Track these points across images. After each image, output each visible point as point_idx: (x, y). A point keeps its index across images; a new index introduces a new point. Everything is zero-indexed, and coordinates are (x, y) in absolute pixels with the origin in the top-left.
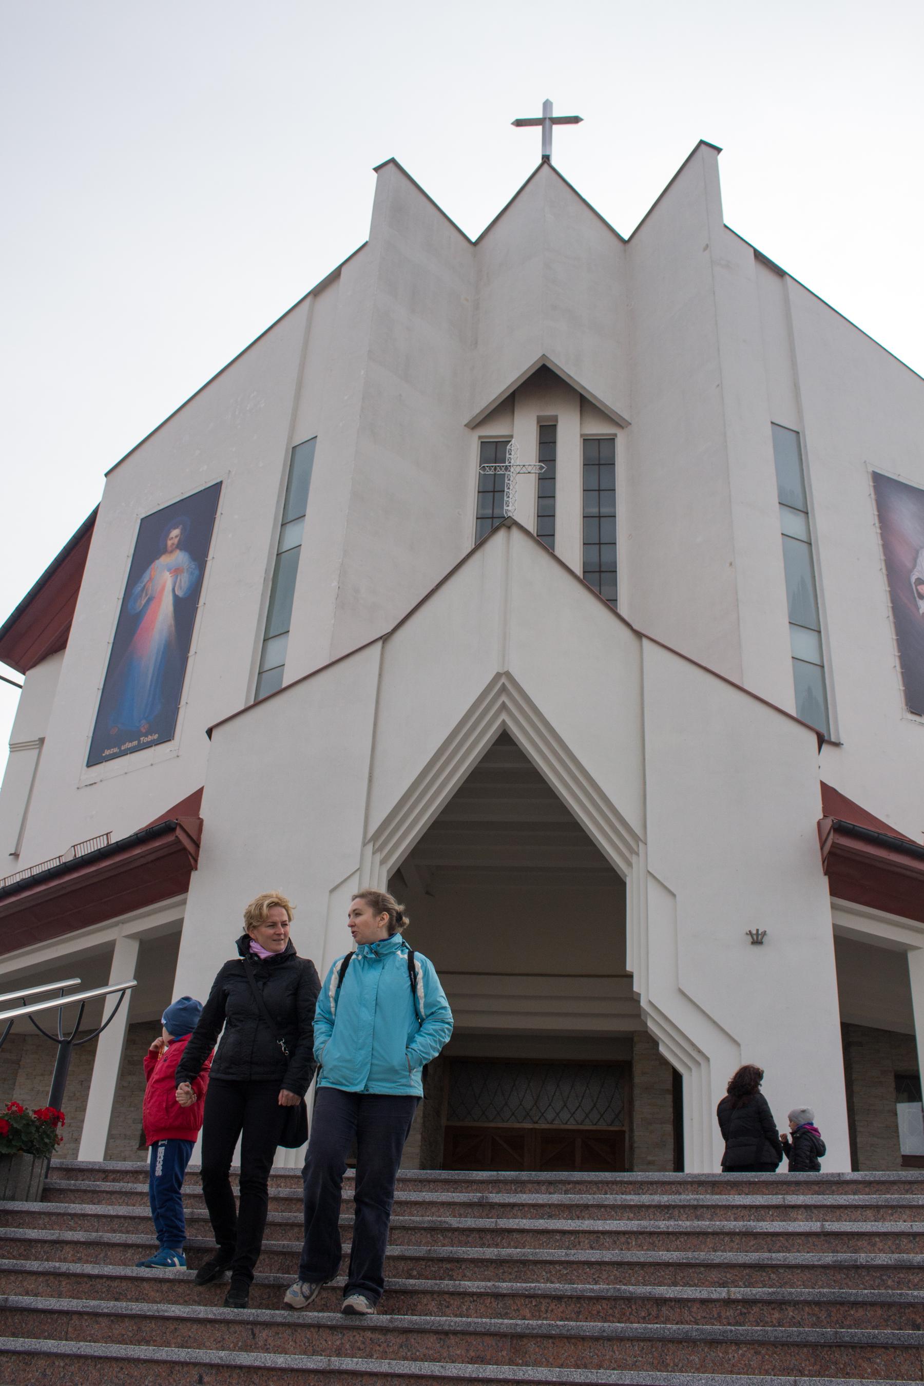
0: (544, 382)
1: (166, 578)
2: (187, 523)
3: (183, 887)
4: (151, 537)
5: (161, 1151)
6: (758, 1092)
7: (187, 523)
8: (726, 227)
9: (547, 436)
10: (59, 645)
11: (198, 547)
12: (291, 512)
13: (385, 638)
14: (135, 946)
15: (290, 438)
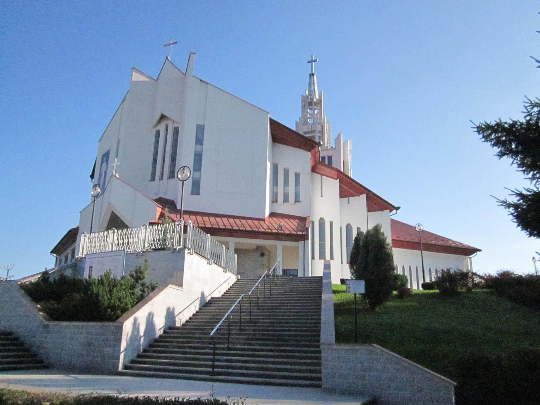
0: (163, 117)
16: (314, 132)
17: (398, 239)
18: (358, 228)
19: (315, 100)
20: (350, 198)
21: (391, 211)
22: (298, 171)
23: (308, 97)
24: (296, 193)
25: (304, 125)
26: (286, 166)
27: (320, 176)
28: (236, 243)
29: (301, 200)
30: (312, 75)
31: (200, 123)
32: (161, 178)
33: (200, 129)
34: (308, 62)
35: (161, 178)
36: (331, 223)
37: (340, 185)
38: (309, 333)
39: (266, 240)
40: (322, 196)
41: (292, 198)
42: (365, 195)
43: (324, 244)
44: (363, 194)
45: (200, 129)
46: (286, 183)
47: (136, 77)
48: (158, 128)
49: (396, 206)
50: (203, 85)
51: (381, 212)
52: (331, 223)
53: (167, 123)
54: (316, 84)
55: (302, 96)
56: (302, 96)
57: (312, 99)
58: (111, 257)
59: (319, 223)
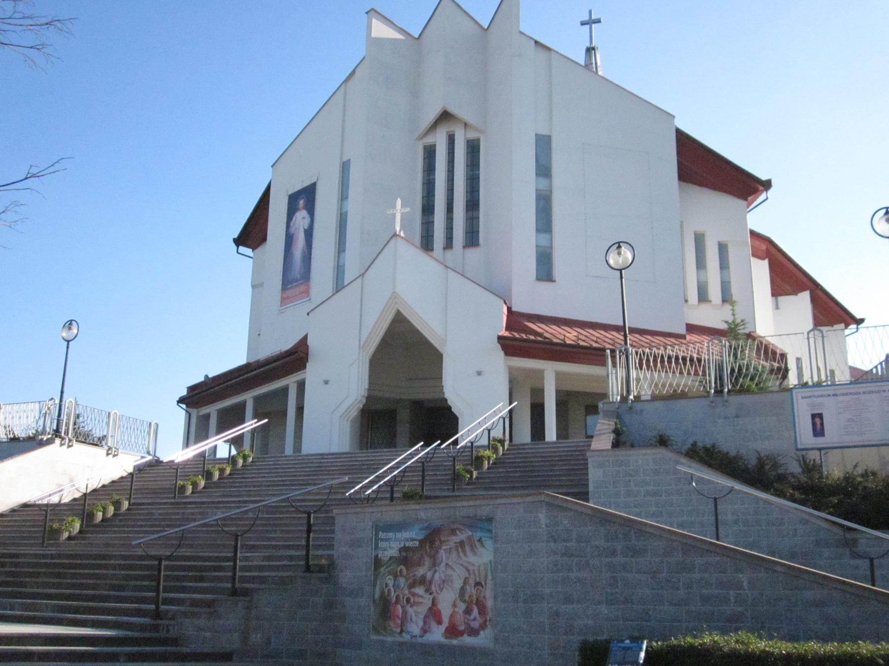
0: (445, 116)
1: (301, 217)
2: (305, 198)
3: (305, 367)
4: (293, 200)
5: (289, 450)
6: (178, 464)
7: (305, 198)
8: (521, 32)
9: (451, 140)
10: (264, 239)
11: (310, 209)
12: (344, 196)
13: (363, 275)
14: (296, 385)
15: (341, 158)
21: (847, 326)
22: (723, 239)
24: (722, 282)
26: (699, 228)
28: (559, 375)
31: (544, 132)
32: (449, 243)
33: (544, 144)
34: (583, 24)
35: (449, 243)
38: (278, 516)
41: (715, 293)
44: (805, 290)
45: (544, 144)
49: (858, 316)
50: (542, 54)
53: (452, 129)
58: (840, 398)
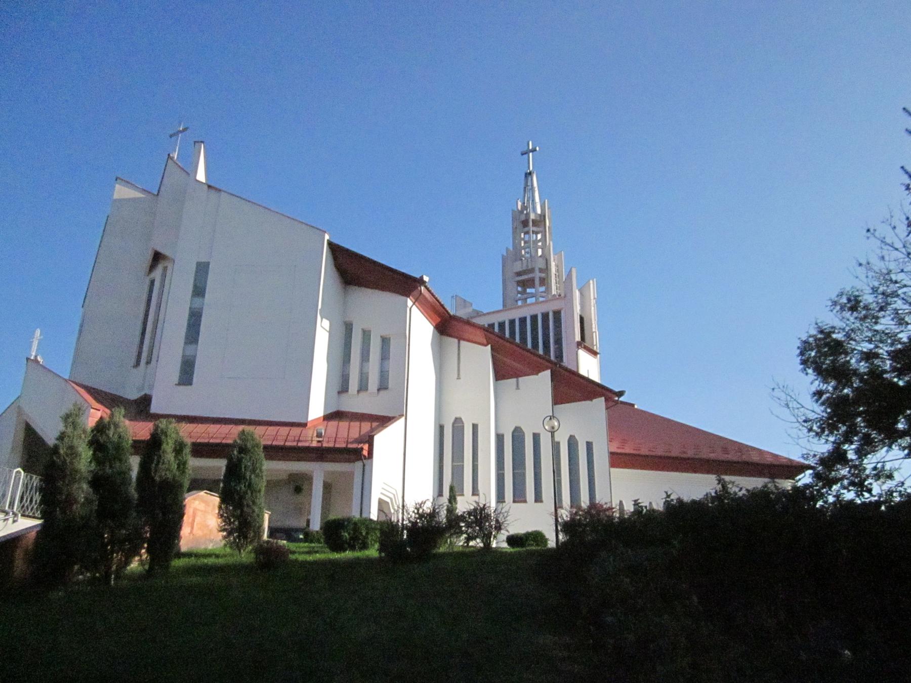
16: (532, 270)
17: (634, 452)
18: (587, 443)
19: (532, 216)
20: (520, 379)
22: (385, 333)
23: (522, 212)
25: (516, 260)
26: (366, 326)
27: (456, 340)
29: (390, 386)
30: (529, 175)
31: (204, 260)
33: (202, 269)
34: (522, 154)
36: (589, 445)
37: (493, 357)
39: (293, 463)
40: (459, 378)
42: (548, 373)
43: (462, 468)
45: (202, 269)
46: (365, 356)
47: (121, 192)
48: (153, 275)
51: (588, 402)
52: (589, 445)
54: (536, 189)
55: (513, 211)
56: (513, 211)
57: (528, 214)
59: (513, 436)
